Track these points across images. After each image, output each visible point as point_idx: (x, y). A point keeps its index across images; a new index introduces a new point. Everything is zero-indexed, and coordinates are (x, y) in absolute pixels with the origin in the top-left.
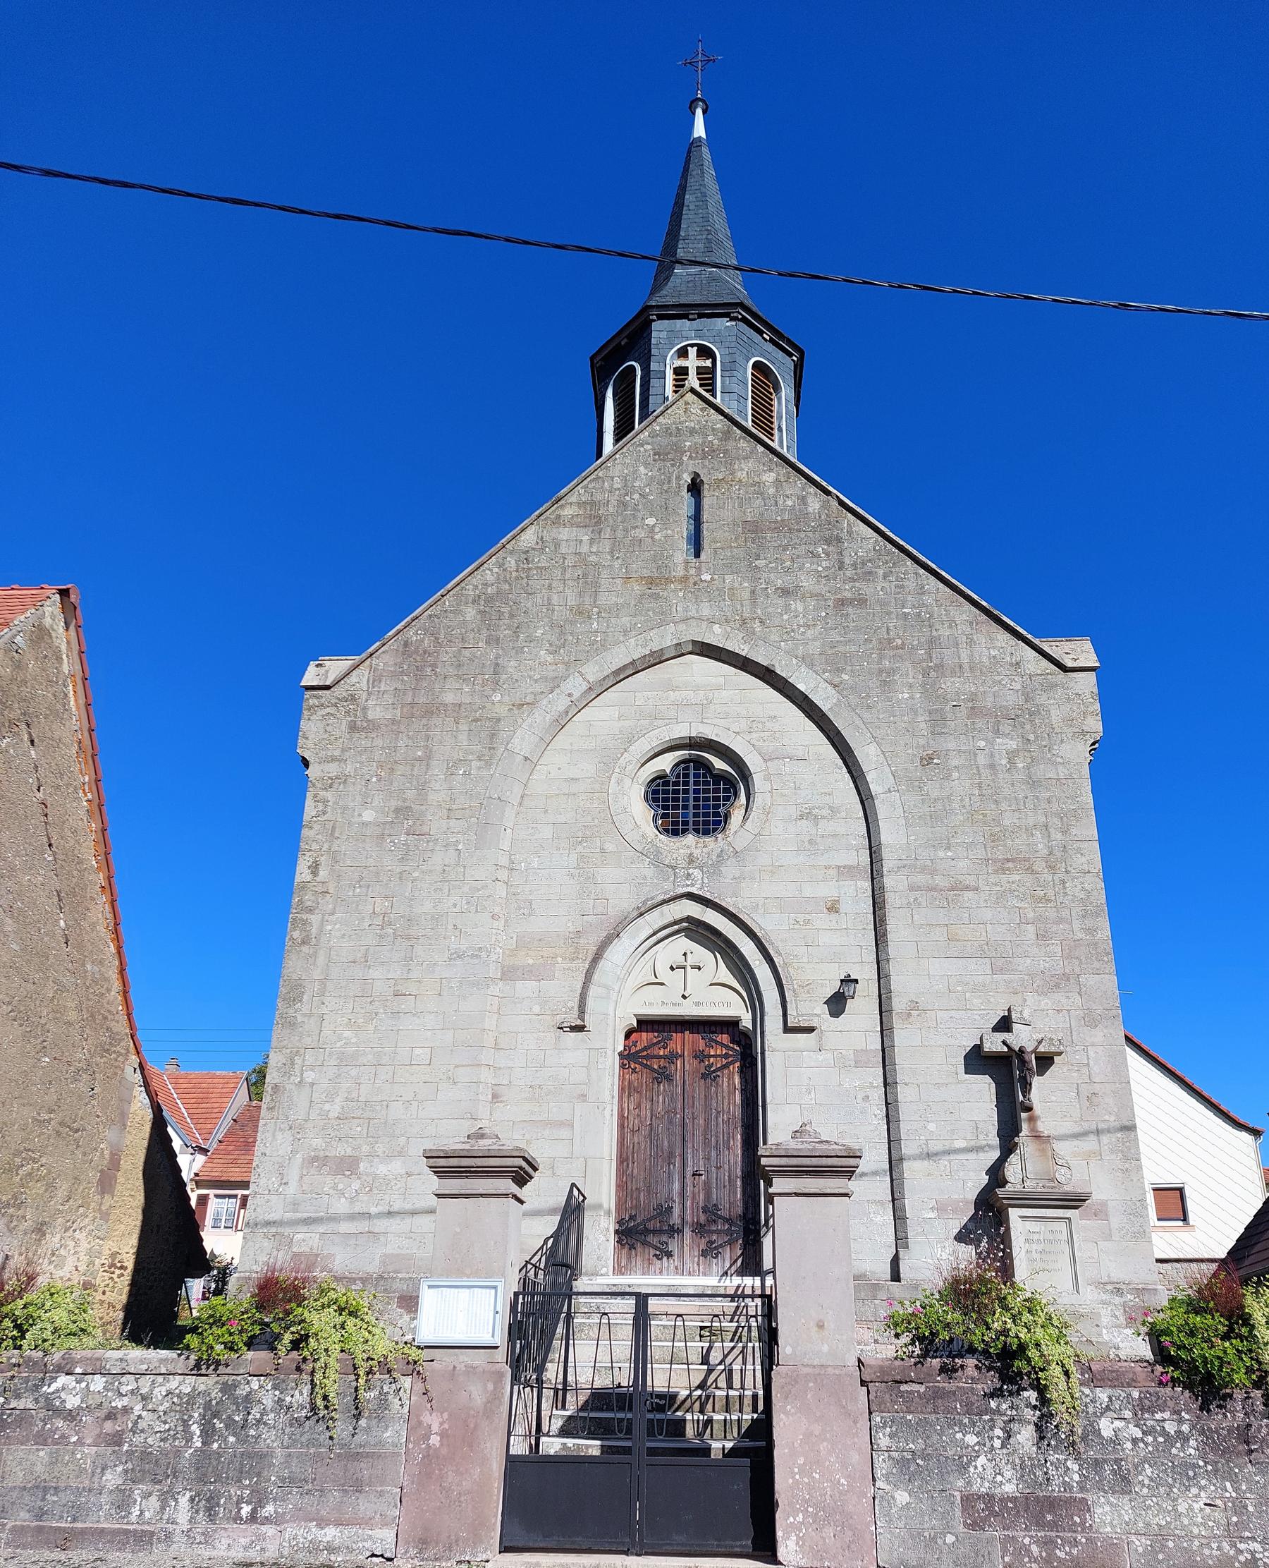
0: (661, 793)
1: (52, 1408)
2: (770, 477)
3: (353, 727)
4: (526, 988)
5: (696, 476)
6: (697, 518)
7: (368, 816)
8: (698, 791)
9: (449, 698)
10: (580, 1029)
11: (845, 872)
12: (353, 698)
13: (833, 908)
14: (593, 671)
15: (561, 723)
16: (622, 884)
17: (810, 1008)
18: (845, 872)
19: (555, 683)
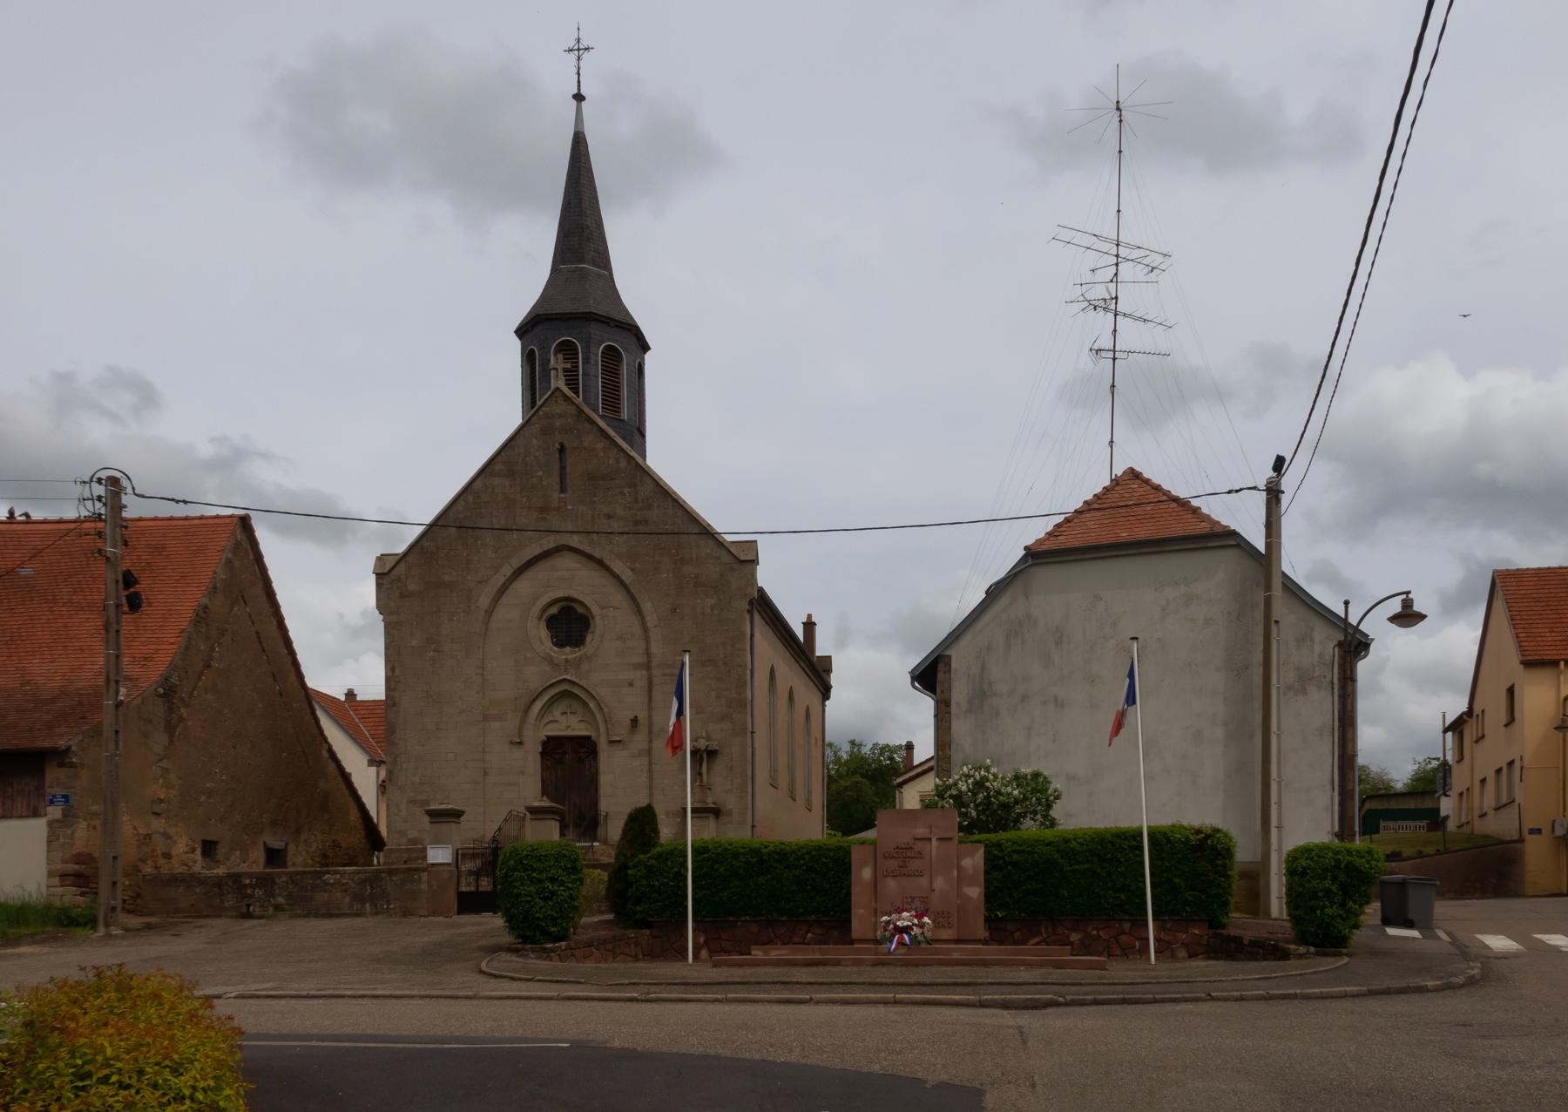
0: (552, 623)
1: (326, 883)
2: (600, 446)
3: (401, 595)
4: (495, 725)
5: (562, 445)
6: (563, 468)
7: (414, 643)
8: (569, 624)
9: (447, 578)
10: (520, 743)
11: (637, 666)
12: (399, 580)
13: (631, 685)
14: (516, 563)
15: (502, 591)
16: (536, 676)
17: (621, 732)
18: (637, 666)
19: (497, 569)
